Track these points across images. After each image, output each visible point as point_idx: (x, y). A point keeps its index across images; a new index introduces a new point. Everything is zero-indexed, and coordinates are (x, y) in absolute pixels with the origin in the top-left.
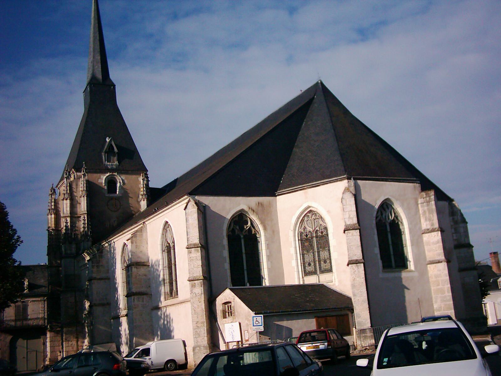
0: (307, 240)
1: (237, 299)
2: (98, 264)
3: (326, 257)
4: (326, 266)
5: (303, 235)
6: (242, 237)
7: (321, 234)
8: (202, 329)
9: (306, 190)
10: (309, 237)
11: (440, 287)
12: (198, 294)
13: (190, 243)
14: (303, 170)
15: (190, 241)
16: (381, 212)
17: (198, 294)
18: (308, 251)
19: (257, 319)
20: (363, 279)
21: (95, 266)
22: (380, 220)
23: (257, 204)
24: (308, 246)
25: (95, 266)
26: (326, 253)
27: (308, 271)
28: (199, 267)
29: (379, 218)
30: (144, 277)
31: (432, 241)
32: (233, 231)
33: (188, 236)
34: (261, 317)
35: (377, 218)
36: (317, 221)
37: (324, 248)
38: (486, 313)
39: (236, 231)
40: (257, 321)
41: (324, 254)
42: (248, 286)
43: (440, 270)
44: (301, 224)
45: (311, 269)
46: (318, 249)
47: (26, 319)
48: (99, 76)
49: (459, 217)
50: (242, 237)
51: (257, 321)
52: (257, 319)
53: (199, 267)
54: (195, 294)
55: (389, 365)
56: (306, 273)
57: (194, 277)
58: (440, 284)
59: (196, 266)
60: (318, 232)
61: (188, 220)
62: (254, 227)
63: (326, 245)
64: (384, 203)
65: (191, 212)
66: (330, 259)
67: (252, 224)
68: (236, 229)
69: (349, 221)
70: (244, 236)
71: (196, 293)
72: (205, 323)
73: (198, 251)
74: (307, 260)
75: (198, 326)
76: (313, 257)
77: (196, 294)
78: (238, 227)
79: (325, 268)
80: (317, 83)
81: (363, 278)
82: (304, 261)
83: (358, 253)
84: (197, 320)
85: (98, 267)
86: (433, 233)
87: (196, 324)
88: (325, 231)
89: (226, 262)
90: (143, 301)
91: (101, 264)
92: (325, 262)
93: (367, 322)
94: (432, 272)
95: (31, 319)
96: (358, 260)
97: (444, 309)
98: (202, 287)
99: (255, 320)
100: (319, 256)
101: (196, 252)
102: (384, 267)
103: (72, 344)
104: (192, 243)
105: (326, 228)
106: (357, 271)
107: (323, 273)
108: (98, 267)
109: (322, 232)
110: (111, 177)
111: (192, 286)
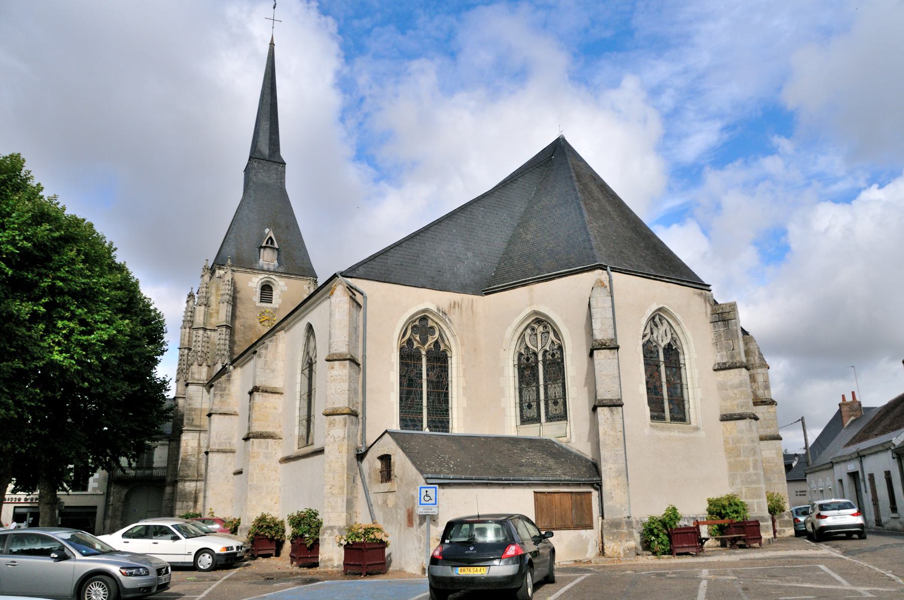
0: (528, 367)
1: (400, 452)
2: (222, 393)
3: (557, 394)
4: (556, 410)
5: (522, 359)
6: (424, 353)
7: (551, 358)
8: (339, 499)
9: (531, 286)
10: (532, 361)
11: (742, 458)
12: (339, 439)
13: (333, 351)
14: (529, 257)
15: (333, 349)
16: (651, 329)
17: (339, 439)
18: (528, 384)
19: (427, 491)
20: (620, 433)
21: (218, 395)
22: (649, 341)
23: (452, 305)
24: (530, 376)
25: (218, 395)
26: (559, 390)
27: (527, 417)
28: (344, 394)
29: (646, 339)
30: (273, 410)
31: (729, 383)
32: (410, 342)
33: (331, 341)
34: (434, 489)
35: (644, 336)
36: (546, 337)
37: (555, 381)
38: (206, 469)
39: (415, 343)
40: (427, 495)
41: (555, 390)
42: (427, 431)
43: (742, 432)
44: (520, 340)
45: (532, 413)
46: (545, 381)
47: (151, 468)
48: (265, 149)
49: (756, 358)
50: (424, 353)
51: (427, 495)
52: (427, 491)
53: (344, 394)
54: (333, 438)
55: (536, 500)
56: (525, 420)
57: (335, 408)
58: (742, 454)
59: (339, 391)
60: (547, 354)
61: (334, 315)
62: (443, 341)
63: (558, 375)
64: (656, 315)
65: (340, 301)
66: (565, 399)
67: (440, 335)
68: (416, 340)
69: (600, 334)
70: (427, 352)
71: (336, 437)
72: (345, 489)
73: (345, 366)
74: (526, 398)
75: (334, 492)
76: (537, 395)
77: (334, 438)
78: (418, 338)
79: (555, 413)
80: (558, 139)
81: (620, 431)
82: (521, 400)
83: (615, 389)
84: (333, 483)
85: (222, 396)
86: (732, 371)
87: (330, 489)
88: (559, 353)
89: (393, 391)
90: (267, 448)
91: (227, 392)
92: (556, 403)
93: (625, 508)
94: (728, 433)
95: (157, 468)
96: (612, 400)
97: (745, 496)
98: (345, 426)
99: (423, 493)
100: (546, 393)
101: (342, 367)
102: (652, 418)
103: (187, 506)
104: (336, 352)
105: (560, 348)
106: (610, 419)
107: (551, 421)
108: (222, 396)
109: (553, 355)
110: (267, 281)
111: (330, 424)
